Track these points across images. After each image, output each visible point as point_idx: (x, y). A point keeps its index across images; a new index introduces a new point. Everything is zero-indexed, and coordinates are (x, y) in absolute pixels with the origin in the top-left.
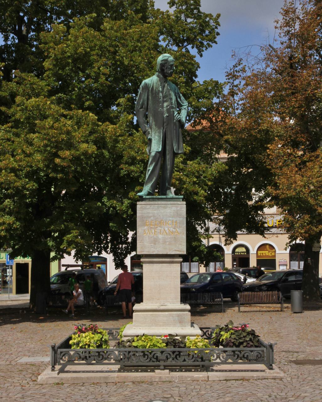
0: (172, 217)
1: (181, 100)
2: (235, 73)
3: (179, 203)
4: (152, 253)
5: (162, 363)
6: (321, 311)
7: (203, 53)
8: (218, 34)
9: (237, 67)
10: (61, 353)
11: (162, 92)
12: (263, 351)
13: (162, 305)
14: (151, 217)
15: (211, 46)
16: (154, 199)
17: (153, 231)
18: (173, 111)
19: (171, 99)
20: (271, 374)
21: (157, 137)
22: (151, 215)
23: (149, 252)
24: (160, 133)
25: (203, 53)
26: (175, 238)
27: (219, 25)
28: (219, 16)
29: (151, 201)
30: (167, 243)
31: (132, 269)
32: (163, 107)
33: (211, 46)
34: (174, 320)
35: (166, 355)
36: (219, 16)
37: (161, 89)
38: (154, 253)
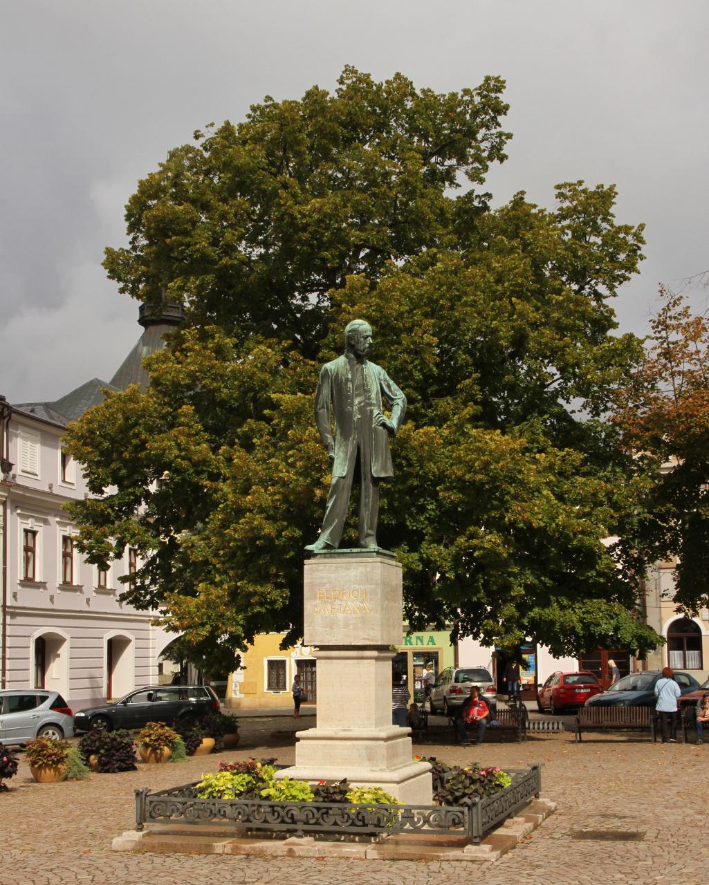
0: (359, 584)
1: (390, 391)
2: (668, 320)
3: (370, 560)
4: (327, 644)
5: (300, 826)
6: (707, 746)
7: (616, 290)
8: (642, 258)
9: (670, 310)
10: (151, 802)
11: (352, 381)
12: (463, 813)
13: (344, 730)
14: (325, 584)
15: (629, 279)
16: (332, 555)
17: (329, 607)
18: (371, 411)
19: (369, 391)
20: (472, 852)
21: (341, 454)
22: (325, 581)
23: (322, 641)
24: (346, 446)
25: (616, 290)
26: (363, 618)
27: (643, 243)
28: (642, 227)
29: (328, 558)
30: (351, 627)
31: (491, 681)
32: (352, 405)
33: (629, 279)
34: (359, 756)
35: (306, 813)
36: (642, 227)
37: (350, 376)
38: (331, 644)
